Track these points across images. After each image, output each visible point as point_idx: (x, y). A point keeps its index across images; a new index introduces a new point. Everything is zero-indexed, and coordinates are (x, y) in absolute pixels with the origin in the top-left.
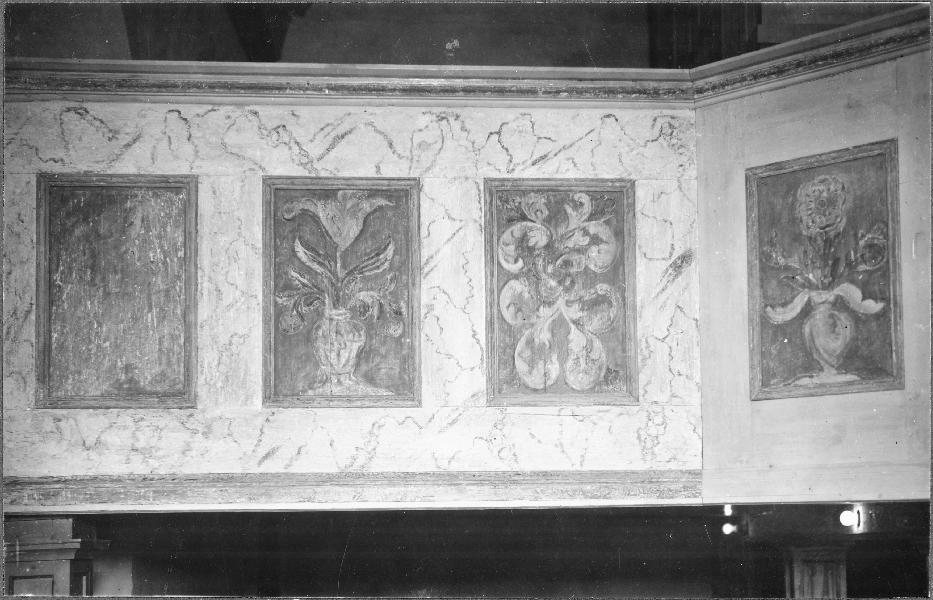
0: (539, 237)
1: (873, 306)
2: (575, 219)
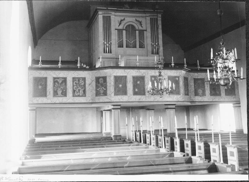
0: (77, 82)
1: (105, 89)
2: (80, 81)
